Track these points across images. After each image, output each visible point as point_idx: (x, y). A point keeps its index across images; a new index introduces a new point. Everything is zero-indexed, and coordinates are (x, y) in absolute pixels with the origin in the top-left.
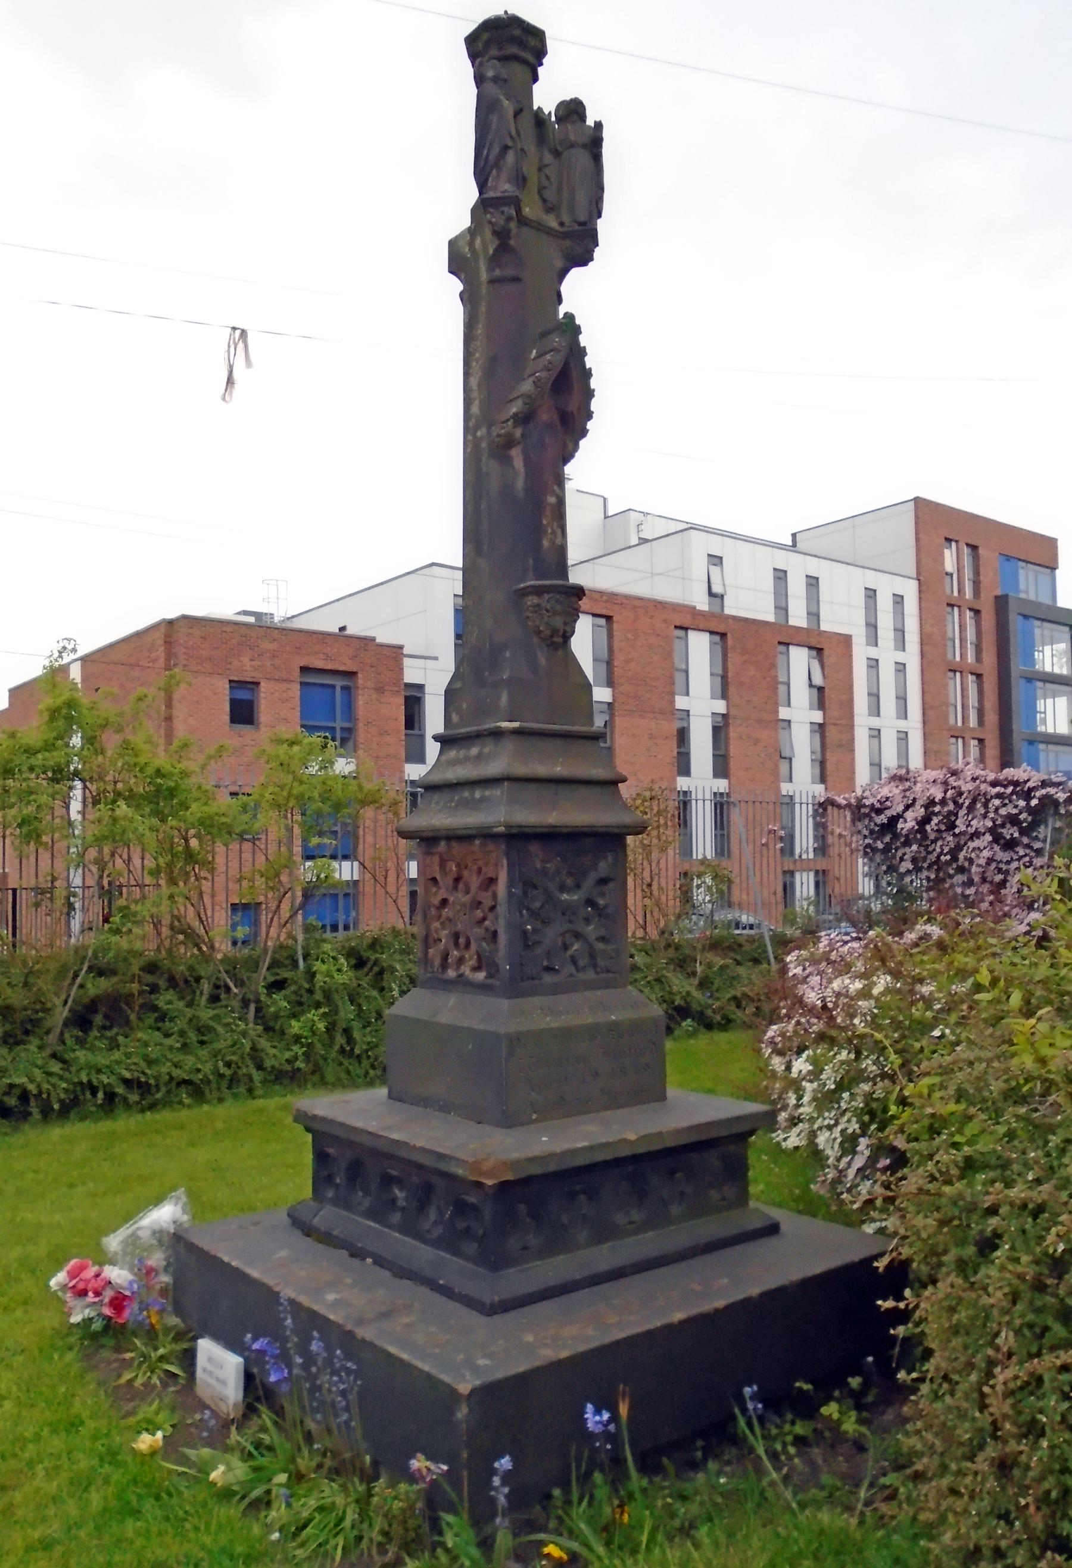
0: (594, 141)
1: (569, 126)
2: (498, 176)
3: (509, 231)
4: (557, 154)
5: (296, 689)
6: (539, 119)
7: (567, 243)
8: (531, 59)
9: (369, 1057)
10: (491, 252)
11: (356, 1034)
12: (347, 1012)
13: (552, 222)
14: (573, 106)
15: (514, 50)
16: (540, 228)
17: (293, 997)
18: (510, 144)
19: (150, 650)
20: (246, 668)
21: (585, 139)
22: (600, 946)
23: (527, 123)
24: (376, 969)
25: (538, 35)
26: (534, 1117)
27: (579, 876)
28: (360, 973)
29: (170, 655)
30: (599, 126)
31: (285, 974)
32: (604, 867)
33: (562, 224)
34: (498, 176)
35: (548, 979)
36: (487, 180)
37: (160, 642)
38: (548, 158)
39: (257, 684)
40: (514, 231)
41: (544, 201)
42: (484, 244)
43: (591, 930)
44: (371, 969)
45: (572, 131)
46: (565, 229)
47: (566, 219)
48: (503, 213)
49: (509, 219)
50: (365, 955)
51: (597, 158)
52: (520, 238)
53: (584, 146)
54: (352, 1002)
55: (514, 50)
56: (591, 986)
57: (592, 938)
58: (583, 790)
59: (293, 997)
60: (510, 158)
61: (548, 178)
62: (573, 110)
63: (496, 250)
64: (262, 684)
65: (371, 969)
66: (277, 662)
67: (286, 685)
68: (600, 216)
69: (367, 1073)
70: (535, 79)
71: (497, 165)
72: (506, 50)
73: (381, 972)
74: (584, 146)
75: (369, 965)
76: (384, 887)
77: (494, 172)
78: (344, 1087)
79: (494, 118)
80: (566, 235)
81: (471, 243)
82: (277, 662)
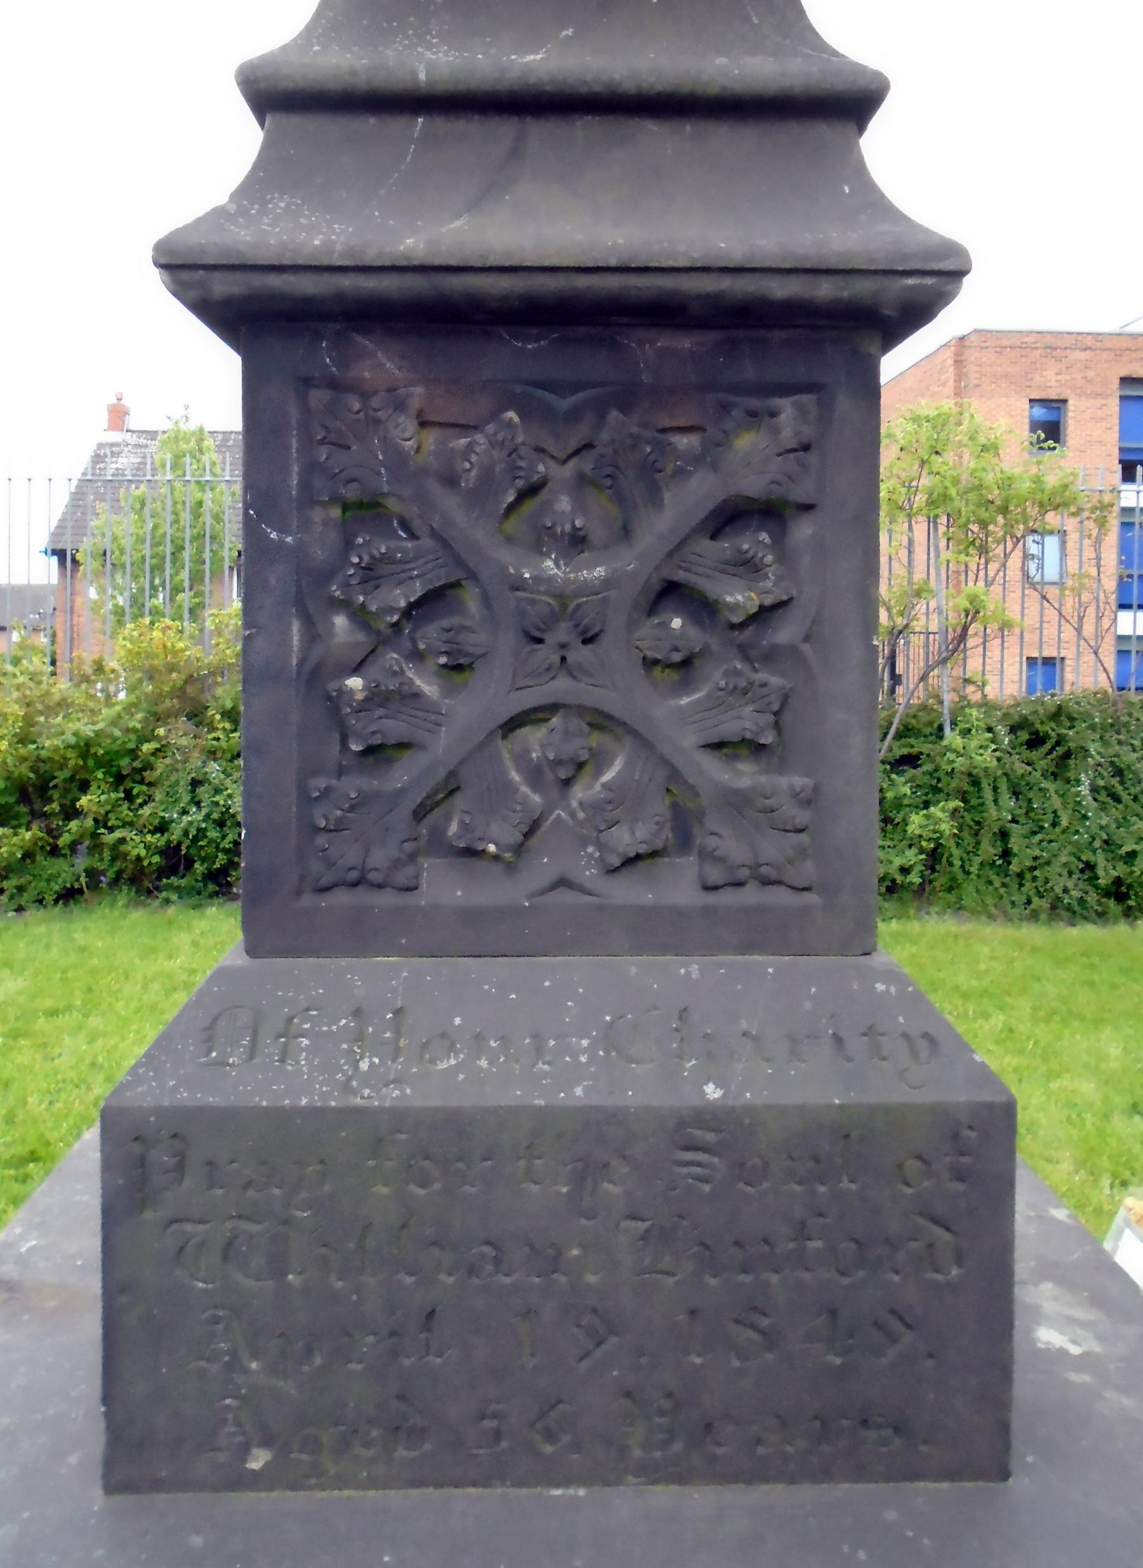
5: (1114, 405)
9: (1034, 879)
11: (1014, 844)
12: (1002, 809)
17: (926, 779)
19: (940, 372)
20: (1051, 383)
22: (716, 773)
24: (1060, 750)
26: (258, 1460)
27: (624, 482)
28: (1034, 755)
29: (959, 377)
31: (919, 746)
32: (752, 458)
35: (443, 887)
37: (950, 362)
39: (1065, 401)
43: (677, 717)
44: (1053, 749)
50: (1042, 729)
54: (1016, 794)
56: (660, 933)
57: (685, 743)
58: (653, 134)
59: (926, 779)
64: (1071, 402)
65: (1053, 749)
66: (1090, 374)
67: (1101, 401)
69: (1029, 902)
73: (1067, 755)
75: (1048, 746)
76: (1079, 630)
78: (990, 917)
82: (1090, 374)
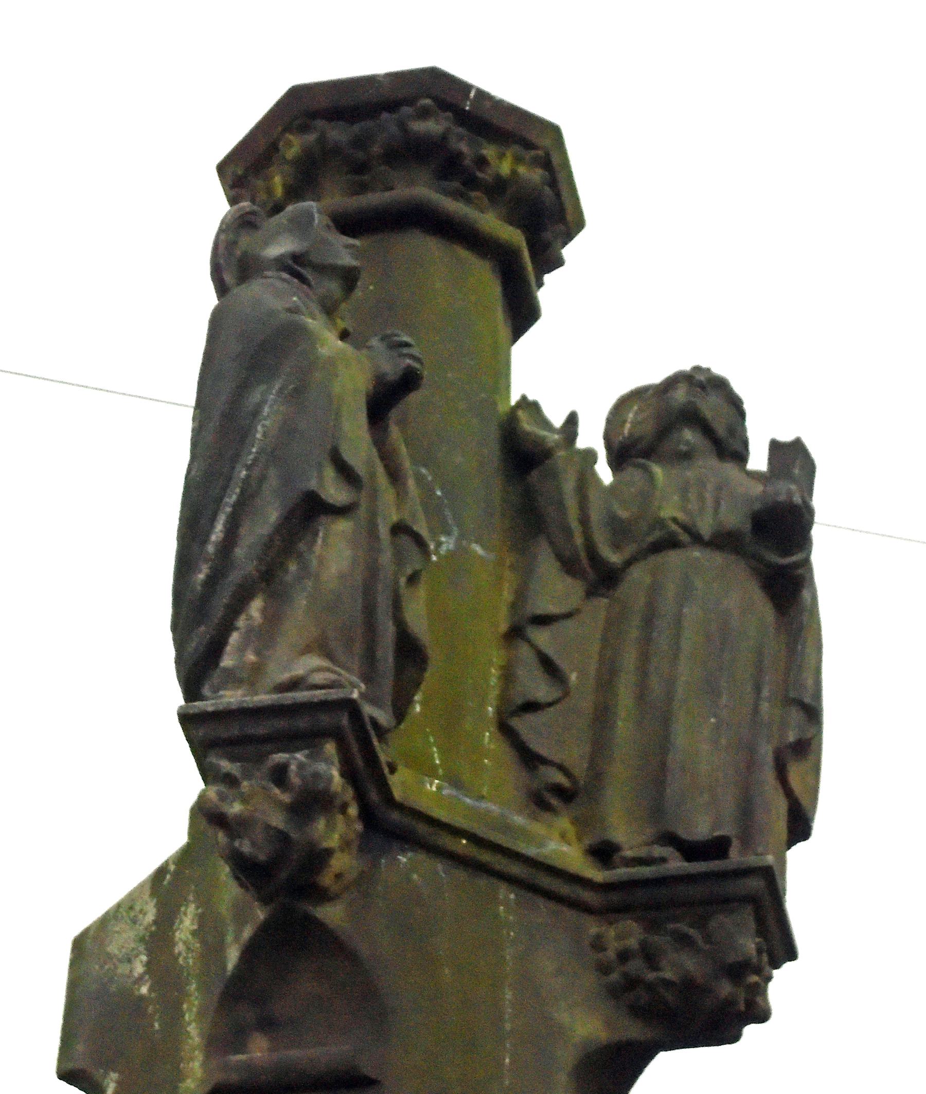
0: (774, 536)
1: (658, 471)
2: (273, 619)
3: (318, 858)
4: (604, 579)
6: (526, 452)
7: (627, 933)
8: (512, 235)
10: (233, 956)
13: (559, 844)
14: (680, 395)
15: (422, 189)
16: (485, 859)
18: (334, 492)
21: (734, 518)
23: (474, 458)
25: (535, 141)
30: (792, 458)
33: (604, 853)
34: (273, 619)
36: (215, 649)
38: (555, 590)
40: (342, 862)
41: (529, 759)
42: (210, 934)
45: (670, 492)
46: (622, 873)
47: (627, 834)
48: (280, 776)
49: (311, 802)
51: (787, 587)
52: (375, 901)
53: (724, 541)
55: (422, 189)
60: (335, 551)
61: (548, 665)
62: (687, 416)
63: (250, 952)
68: (799, 827)
70: (522, 314)
71: (269, 578)
72: (398, 197)
74: (724, 541)
77: (256, 607)
79: (269, 409)
80: (620, 900)
81: (159, 939)
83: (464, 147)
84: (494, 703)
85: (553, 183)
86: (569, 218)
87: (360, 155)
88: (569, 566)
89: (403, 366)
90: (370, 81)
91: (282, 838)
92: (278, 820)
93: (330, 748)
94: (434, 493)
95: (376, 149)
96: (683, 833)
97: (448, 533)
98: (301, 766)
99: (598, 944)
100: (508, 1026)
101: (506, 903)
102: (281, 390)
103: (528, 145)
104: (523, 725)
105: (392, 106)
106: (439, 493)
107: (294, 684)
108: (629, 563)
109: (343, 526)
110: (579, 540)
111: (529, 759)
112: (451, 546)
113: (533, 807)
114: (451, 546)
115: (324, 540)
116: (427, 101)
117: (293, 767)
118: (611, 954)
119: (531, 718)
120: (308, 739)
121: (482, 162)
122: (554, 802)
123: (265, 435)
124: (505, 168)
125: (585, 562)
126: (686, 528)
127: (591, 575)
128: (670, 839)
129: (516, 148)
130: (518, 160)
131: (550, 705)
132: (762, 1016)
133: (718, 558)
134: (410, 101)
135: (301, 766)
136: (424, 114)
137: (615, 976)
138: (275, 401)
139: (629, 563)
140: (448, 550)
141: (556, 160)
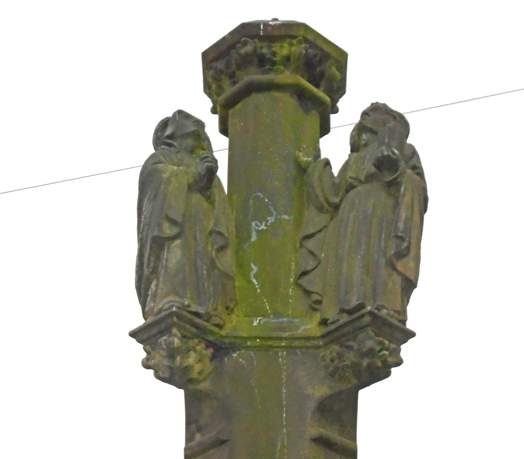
15: (253, 75)
53: (370, 178)
55: (253, 75)
68: (410, 285)
83: (265, 51)
84: (294, 276)
85: (313, 45)
86: (334, 54)
87: (230, 71)
88: (321, 209)
89: (205, 166)
90: (224, 39)
91: (170, 367)
92: (166, 362)
93: (175, 331)
94: (264, 201)
95: (234, 67)
96: (346, 308)
97: (271, 215)
98: (165, 341)
99: (323, 359)
100: (284, 402)
101: (282, 357)
102: (149, 198)
103: (293, 37)
104: (304, 282)
105: (233, 46)
106: (267, 200)
107: (160, 311)
108: (341, 201)
109: (177, 242)
110: (322, 199)
111: (308, 293)
112: (273, 221)
113: (311, 311)
114: (273, 221)
115: (168, 252)
116: (244, 39)
117: (163, 342)
118: (328, 361)
119: (306, 278)
120: (166, 331)
121: (274, 54)
122: (317, 307)
123: (145, 218)
124: (285, 52)
125: (326, 206)
126: (355, 179)
127: (331, 209)
128: (343, 311)
129: (288, 40)
130: (291, 45)
131: (313, 270)
132: (399, 363)
133: (368, 186)
134: (238, 42)
135: (165, 341)
136: (245, 44)
137: (331, 369)
138: (147, 203)
139: (341, 201)
140: (271, 223)
141: (310, 37)
